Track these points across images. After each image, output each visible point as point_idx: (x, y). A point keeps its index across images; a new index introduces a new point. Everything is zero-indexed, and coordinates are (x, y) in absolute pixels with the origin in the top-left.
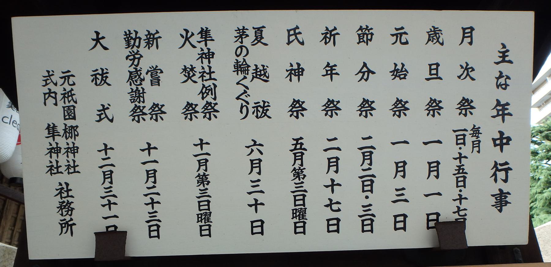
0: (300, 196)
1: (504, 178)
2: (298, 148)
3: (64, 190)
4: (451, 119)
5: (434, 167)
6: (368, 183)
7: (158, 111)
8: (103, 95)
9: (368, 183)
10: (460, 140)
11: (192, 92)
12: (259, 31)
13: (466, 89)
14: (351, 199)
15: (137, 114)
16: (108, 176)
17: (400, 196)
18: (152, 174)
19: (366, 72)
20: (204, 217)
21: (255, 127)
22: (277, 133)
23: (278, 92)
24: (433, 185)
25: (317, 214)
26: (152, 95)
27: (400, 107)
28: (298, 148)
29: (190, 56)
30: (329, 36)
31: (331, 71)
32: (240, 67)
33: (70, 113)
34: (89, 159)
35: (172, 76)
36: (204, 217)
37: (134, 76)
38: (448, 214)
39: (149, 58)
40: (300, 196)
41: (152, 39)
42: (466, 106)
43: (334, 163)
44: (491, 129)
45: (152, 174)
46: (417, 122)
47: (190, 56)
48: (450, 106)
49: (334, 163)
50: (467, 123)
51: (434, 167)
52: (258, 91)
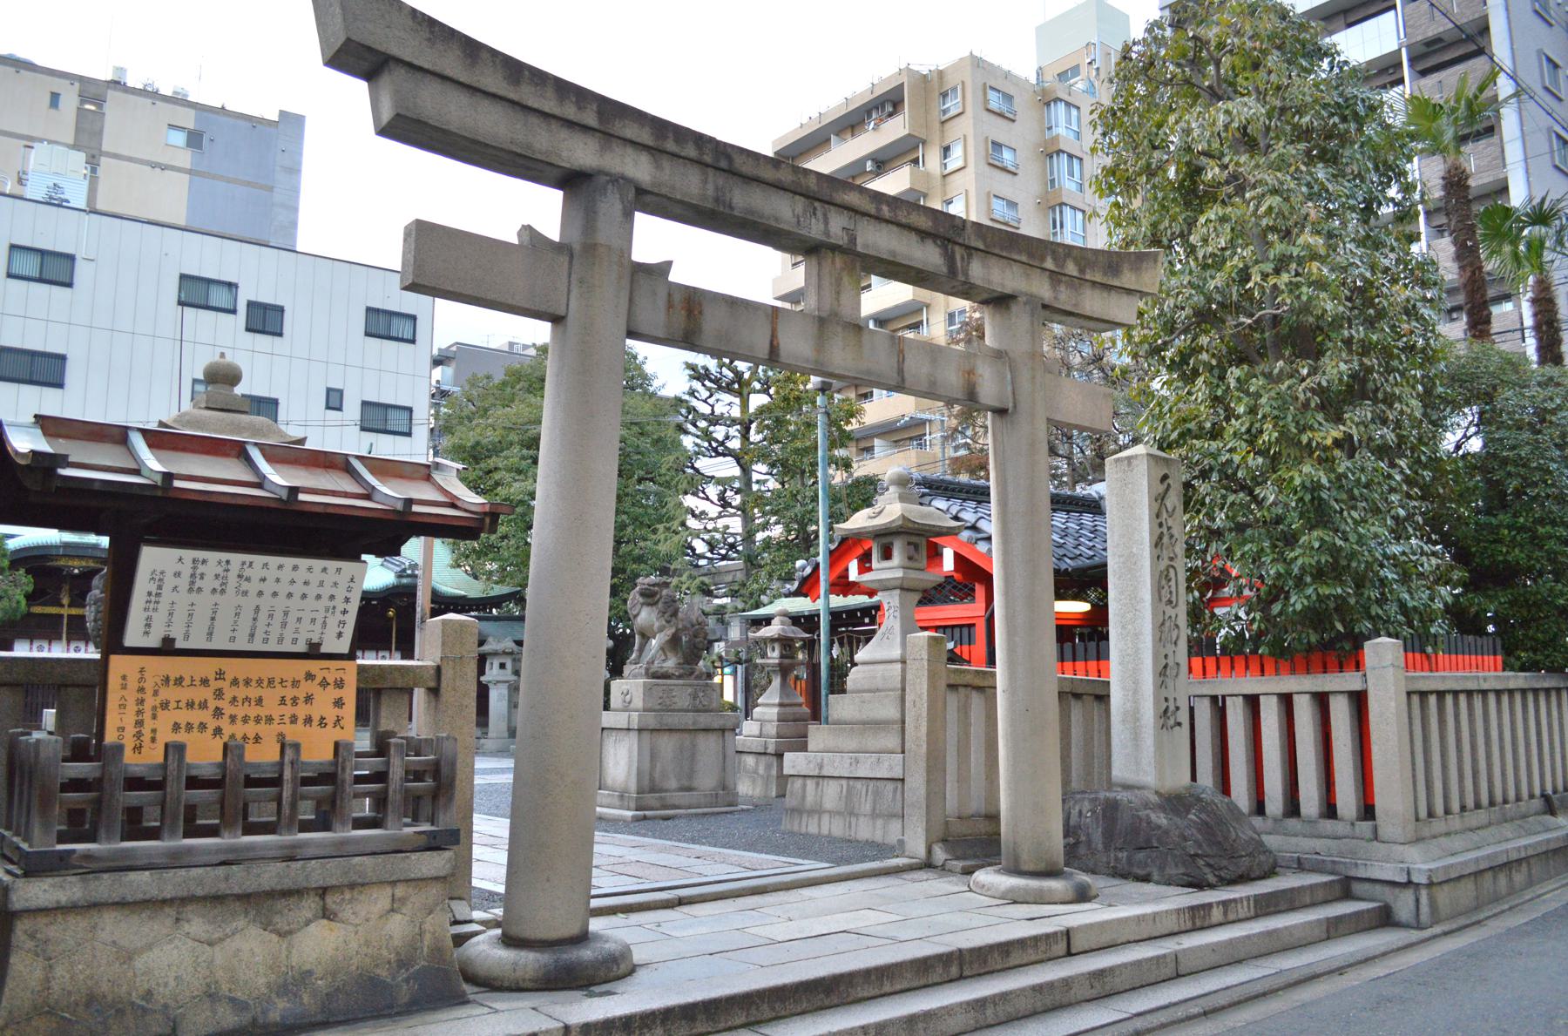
0: (254, 628)
1: (432, 684)
2: (257, 609)
3: (149, 618)
4: (325, 602)
5: (313, 621)
6: (284, 625)
7: (200, 589)
8: (177, 581)
9: (284, 625)
10: (327, 610)
11: (217, 584)
12: (251, 564)
13: (333, 591)
14: (275, 630)
15: (190, 590)
16: (171, 614)
17: (297, 631)
18: (191, 615)
19: (293, 582)
20: (210, 634)
21: (241, 600)
22: (249, 603)
23: (253, 587)
24: (311, 627)
25: (259, 635)
26: (199, 583)
27: (304, 596)
28: (257, 609)
29: (220, 570)
30: (280, 567)
31: (306, 583)
32: (240, 576)
33: (160, 587)
34: (164, 607)
35: (209, 577)
36: (210, 634)
37: (193, 575)
38: (315, 640)
39: (201, 569)
40: (254, 628)
41: (204, 562)
42: (332, 597)
43: (271, 616)
44: (341, 607)
45: (191, 615)
46: (311, 602)
47: (220, 570)
48: (325, 597)
49: (271, 616)
50: (331, 604)
51: (313, 621)
52: (245, 586)
